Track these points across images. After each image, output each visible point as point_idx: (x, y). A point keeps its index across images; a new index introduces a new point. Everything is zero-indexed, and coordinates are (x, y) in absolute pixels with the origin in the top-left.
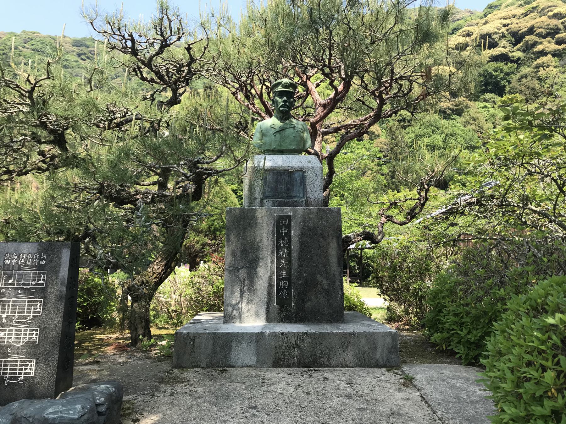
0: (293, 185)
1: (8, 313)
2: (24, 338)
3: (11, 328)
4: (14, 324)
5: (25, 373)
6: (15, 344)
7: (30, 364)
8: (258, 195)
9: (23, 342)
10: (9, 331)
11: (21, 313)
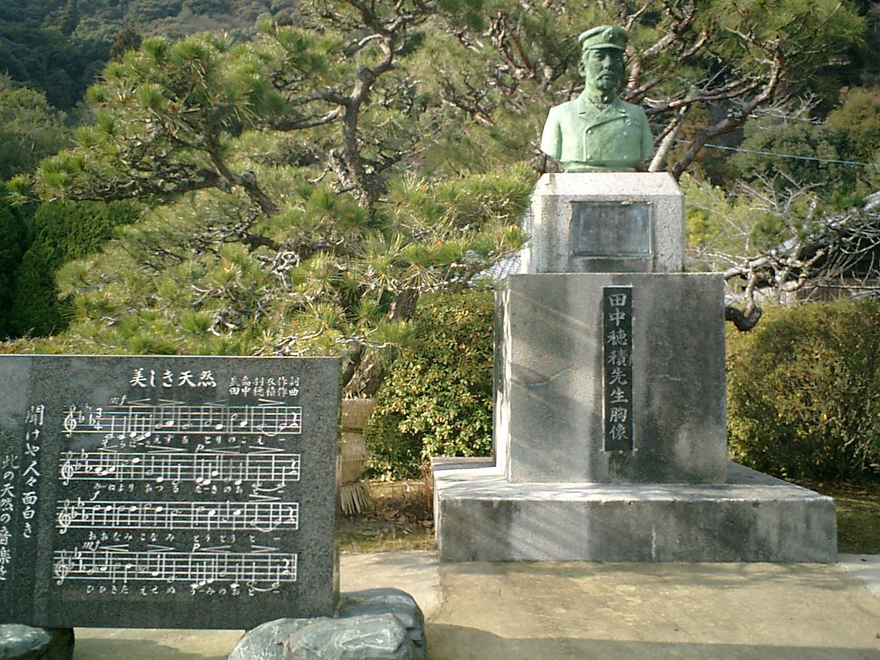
0: (629, 231)
1: (243, 477)
2: (274, 519)
3: (251, 503)
4: (256, 495)
5: (281, 577)
6: (260, 529)
7: (288, 562)
8: (564, 250)
9: (273, 525)
10: (249, 507)
11: (265, 477)
